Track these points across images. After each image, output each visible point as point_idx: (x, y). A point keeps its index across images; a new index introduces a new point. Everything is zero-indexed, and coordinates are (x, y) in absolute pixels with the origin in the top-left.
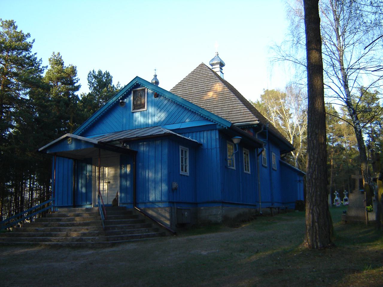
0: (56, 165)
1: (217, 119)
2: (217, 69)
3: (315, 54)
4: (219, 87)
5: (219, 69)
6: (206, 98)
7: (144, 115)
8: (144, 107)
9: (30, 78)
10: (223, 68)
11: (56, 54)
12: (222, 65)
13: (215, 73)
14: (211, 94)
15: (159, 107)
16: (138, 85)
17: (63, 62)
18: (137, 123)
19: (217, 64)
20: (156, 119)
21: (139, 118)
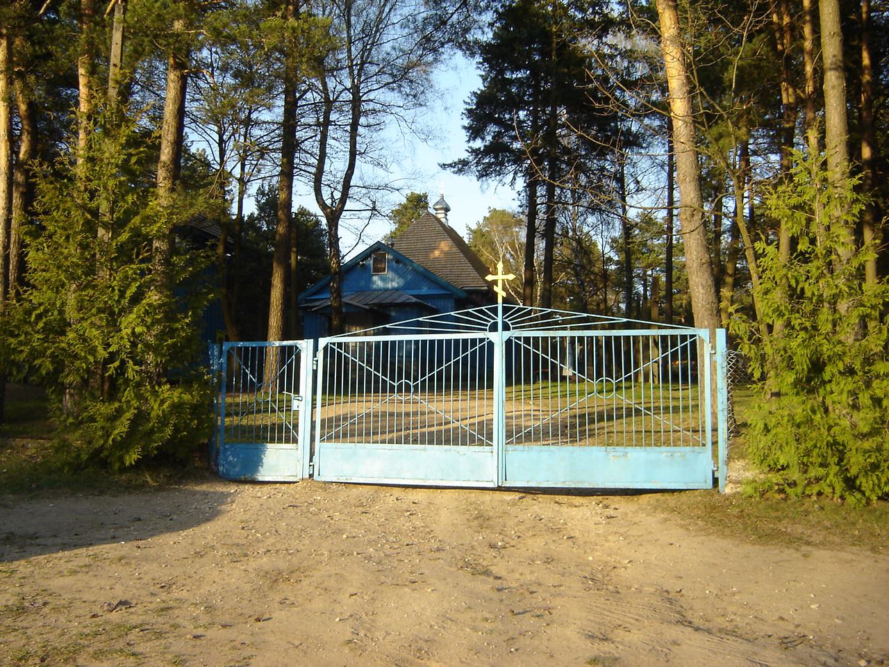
0: (311, 449)
1: (454, 289)
2: (441, 216)
3: (317, 184)
4: (445, 245)
5: (443, 215)
6: (432, 256)
7: (384, 280)
8: (384, 271)
9: (861, 40)
10: (448, 213)
11: (201, 149)
12: (447, 210)
13: (438, 220)
14: (437, 253)
15: (400, 274)
16: (379, 249)
17: (637, 217)
18: (374, 286)
19: (441, 209)
20: (395, 285)
21: (378, 282)
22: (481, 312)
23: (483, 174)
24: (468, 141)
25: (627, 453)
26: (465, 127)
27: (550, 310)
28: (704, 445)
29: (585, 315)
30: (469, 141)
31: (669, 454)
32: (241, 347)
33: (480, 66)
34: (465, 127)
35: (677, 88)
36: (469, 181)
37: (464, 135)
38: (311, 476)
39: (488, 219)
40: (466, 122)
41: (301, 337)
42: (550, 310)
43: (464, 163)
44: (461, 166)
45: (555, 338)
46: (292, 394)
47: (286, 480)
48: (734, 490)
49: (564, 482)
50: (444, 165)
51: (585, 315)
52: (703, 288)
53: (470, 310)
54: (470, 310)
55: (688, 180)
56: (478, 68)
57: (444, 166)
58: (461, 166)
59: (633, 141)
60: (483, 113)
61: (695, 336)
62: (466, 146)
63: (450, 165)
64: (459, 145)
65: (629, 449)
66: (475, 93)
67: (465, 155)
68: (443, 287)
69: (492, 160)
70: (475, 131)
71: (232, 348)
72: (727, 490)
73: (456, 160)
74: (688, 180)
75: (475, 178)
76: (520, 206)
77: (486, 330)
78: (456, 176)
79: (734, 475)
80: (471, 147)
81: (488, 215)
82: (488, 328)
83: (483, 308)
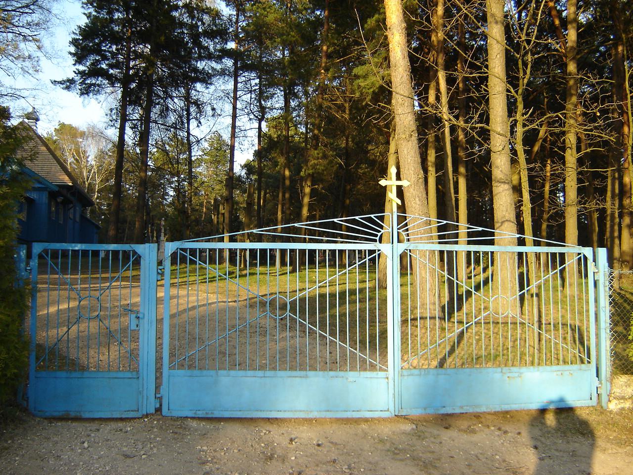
10: (38, 123)
22: (370, 220)
23: (86, 91)
24: (74, 65)
25: (521, 373)
26: (70, 53)
27: (445, 222)
28: (589, 362)
29: (480, 229)
30: (74, 65)
31: (559, 373)
32: (78, 251)
33: (85, 6)
34: (70, 53)
35: (397, 23)
36: (73, 97)
37: (71, 60)
38: (159, 410)
39: (58, 130)
40: (73, 49)
41: (143, 240)
42: (445, 222)
43: (72, 81)
44: (68, 84)
45: (478, 252)
46: (357, 352)
47: (123, 416)
48: (619, 406)
49: (462, 407)
50: (55, 81)
51: (480, 229)
52: (419, 200)
53: (357, 218)
54: (357, 218)
55: (406, 104)
56: (83, 7)
57: (55, 82)
58: (68, 84)
59: (206, 78)
60: (87, 44)
61: (580, 254)
62: (74, 68)
63: (60, 83)
64: (68, 68)
65: (524, 369)
66: (80, 27)
67: (71, 75)
68: (40, 183)
69: (86, 84)
70: (80, 58)
71: (46, 251)
72: (613, 406)
73: (65, 79)
74: (406, 104)
75: (78, 96)
76: (111, 121)
77: (375, 241)
78: (66, 91)
79: (617, 391)
80: (78, 70)
81: (58, 127)
82: (377, 238)
83: (372, 216)
